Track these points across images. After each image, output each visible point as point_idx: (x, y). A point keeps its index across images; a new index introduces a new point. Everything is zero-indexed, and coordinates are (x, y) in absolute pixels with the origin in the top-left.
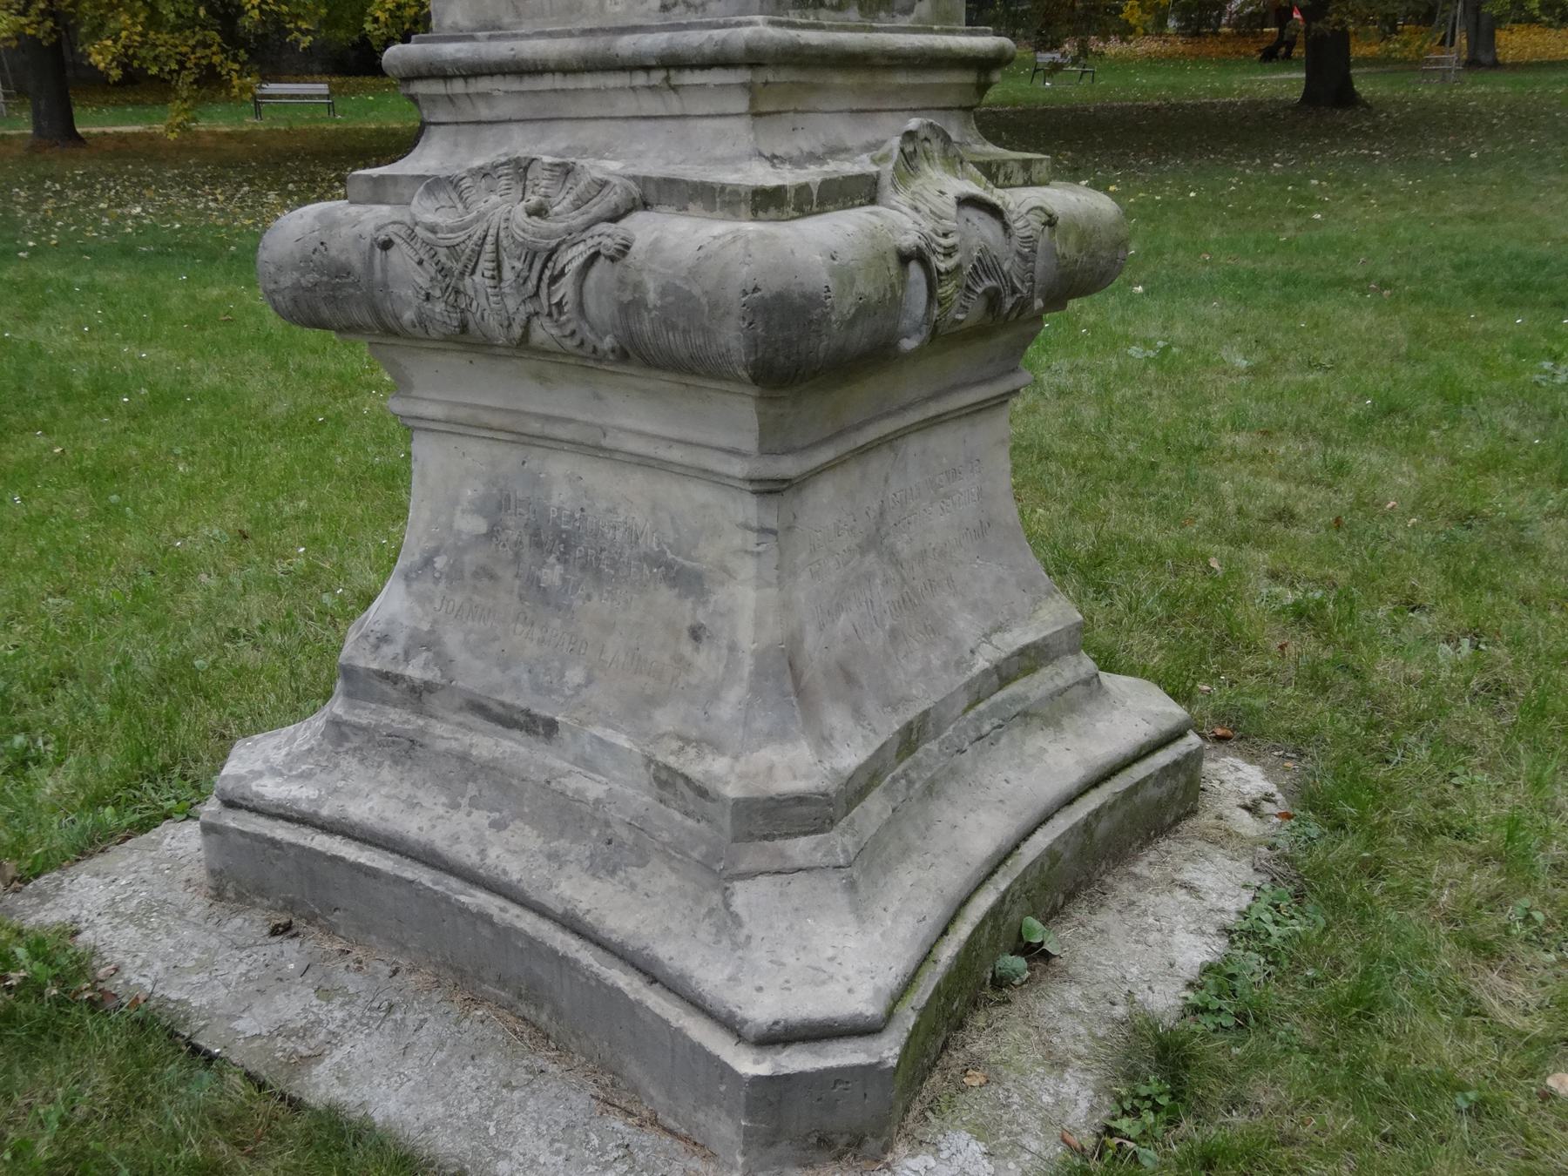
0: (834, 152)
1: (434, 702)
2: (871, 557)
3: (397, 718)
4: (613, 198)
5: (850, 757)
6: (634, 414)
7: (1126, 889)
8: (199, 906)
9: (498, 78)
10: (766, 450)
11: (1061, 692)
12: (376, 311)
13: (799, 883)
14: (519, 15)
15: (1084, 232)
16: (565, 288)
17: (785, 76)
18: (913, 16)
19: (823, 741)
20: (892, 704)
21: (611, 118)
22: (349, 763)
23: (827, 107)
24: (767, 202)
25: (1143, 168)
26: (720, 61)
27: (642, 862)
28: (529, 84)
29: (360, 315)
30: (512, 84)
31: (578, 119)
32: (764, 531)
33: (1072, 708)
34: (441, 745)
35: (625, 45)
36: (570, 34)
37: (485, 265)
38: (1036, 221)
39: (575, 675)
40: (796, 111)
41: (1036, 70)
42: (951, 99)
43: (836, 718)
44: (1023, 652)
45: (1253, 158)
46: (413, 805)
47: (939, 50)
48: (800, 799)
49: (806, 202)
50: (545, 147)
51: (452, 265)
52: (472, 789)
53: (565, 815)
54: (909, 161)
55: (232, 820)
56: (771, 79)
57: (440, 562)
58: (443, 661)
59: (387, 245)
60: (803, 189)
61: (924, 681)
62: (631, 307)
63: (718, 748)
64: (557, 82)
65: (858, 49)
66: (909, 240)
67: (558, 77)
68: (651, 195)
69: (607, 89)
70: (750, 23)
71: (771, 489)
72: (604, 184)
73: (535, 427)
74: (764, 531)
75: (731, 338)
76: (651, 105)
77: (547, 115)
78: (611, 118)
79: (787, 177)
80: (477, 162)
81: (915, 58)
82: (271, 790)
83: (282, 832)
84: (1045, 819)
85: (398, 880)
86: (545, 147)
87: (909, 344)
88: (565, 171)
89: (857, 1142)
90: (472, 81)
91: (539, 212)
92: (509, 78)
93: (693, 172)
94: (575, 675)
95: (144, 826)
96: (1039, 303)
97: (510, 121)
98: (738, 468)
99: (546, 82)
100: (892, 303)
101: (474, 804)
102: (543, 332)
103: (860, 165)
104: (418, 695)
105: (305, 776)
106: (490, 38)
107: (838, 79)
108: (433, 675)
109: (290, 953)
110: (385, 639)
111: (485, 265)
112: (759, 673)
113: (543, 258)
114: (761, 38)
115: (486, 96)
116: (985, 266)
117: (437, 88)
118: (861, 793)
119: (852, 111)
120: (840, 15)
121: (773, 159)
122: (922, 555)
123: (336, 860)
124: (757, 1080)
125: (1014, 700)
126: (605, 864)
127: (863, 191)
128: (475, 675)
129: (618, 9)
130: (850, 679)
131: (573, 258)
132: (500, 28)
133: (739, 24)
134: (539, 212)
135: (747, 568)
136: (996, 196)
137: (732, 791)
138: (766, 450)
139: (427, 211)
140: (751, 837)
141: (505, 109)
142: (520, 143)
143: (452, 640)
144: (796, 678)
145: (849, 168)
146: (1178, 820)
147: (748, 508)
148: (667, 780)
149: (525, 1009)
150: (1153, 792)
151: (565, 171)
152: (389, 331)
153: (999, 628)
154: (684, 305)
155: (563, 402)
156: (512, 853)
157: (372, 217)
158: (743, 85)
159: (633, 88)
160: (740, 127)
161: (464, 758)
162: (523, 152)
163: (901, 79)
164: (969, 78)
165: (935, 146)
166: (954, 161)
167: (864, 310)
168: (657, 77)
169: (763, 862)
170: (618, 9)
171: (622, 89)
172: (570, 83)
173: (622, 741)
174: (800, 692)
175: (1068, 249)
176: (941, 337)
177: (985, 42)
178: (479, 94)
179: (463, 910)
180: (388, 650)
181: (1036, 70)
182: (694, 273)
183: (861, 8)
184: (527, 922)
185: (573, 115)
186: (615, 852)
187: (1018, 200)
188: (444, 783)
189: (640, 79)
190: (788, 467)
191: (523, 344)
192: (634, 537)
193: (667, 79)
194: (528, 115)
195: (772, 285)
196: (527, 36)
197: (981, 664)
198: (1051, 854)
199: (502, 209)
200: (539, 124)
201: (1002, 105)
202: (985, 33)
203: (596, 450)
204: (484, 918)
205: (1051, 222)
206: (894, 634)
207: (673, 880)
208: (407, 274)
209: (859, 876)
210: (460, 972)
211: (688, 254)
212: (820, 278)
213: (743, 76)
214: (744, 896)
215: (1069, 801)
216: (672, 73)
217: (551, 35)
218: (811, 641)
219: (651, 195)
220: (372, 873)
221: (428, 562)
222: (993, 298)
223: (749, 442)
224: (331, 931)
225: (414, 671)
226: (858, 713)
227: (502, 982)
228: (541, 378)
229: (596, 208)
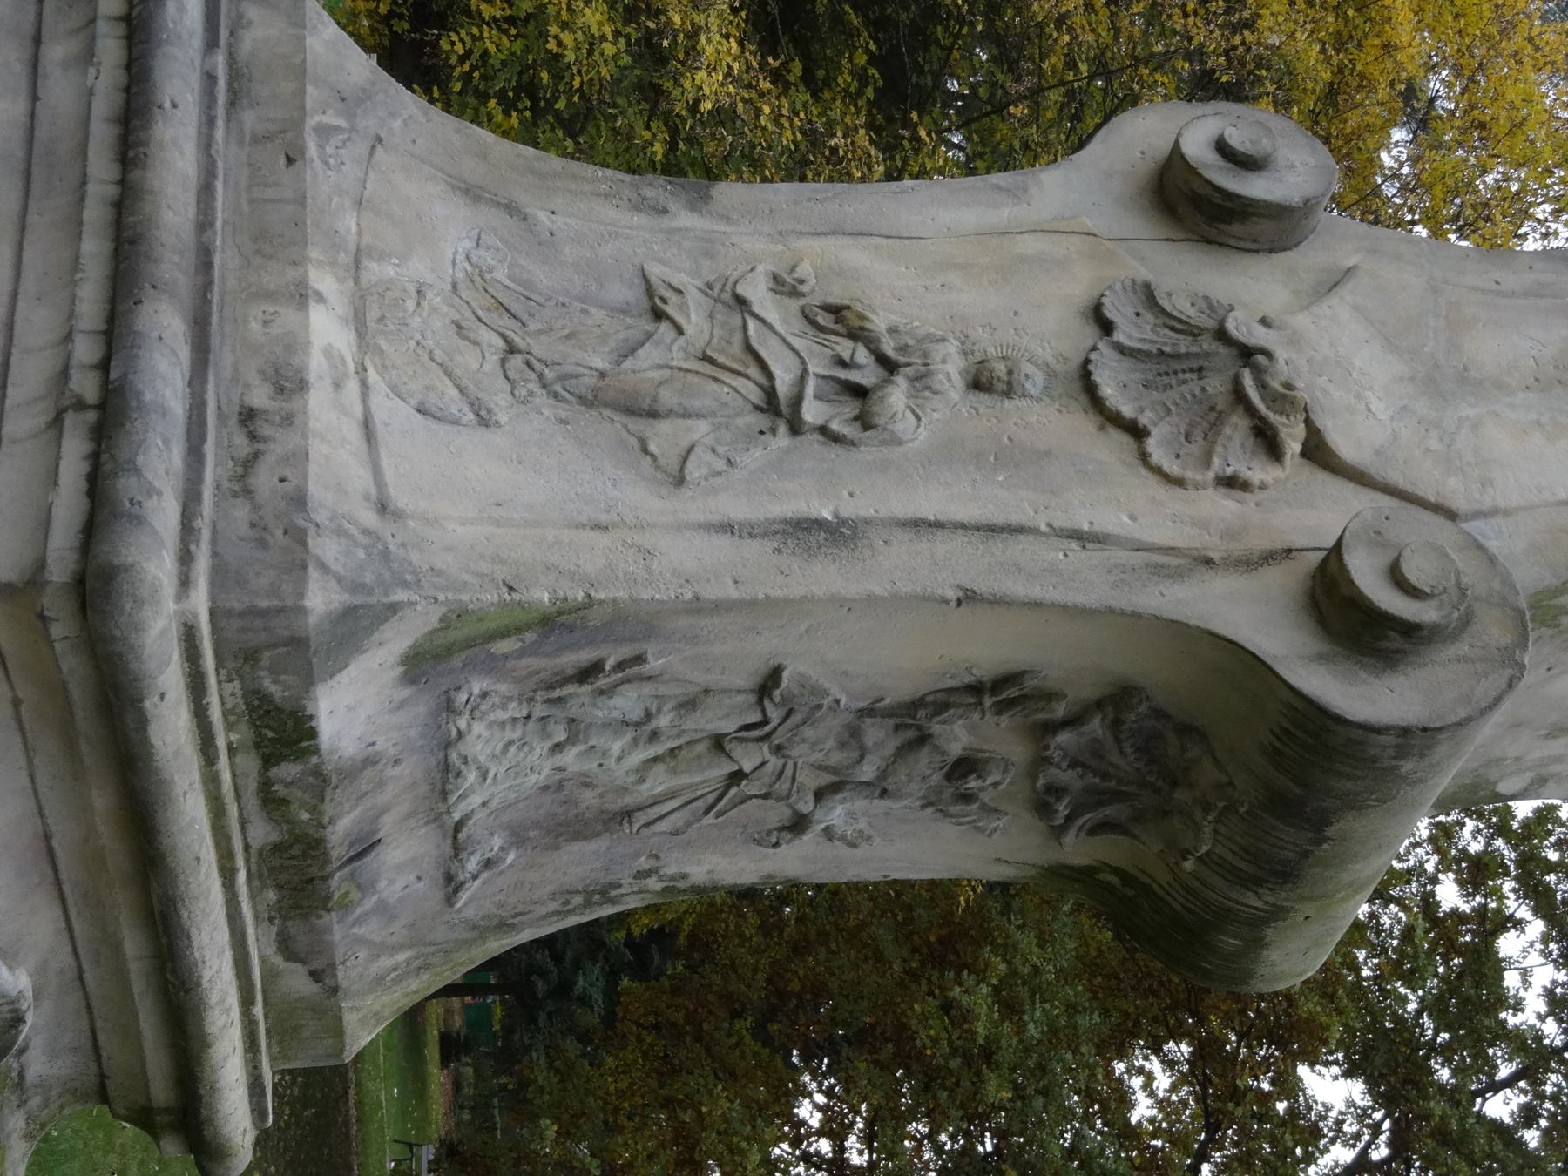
9: (121, 77)
14: (255, 140)
18: (278, 961)
21: (14, 295)
23: (43, 781)
26: (103, 508)
28: (102, 134)
30: (104, 104)
31: (23, 229)
35: (164, 324)
36: (204, 223)
40: (16, 703)
41: (410, 1145)
47: (201, 1025)
56: (57, 630)
65: (166, 842)
67: (112, 191)
69: (74, 283)
70: (185, 583)
77: (35, 169)
78: (14, 295)
81: (174, 971)
90: (121, 29)
92: (120, 98)
97: (35, 98)
99: (101, 169)
106: (210, 78)
107: (102, 799)
114: (139, 603)
115: (88, 56)
119: (47, 837)
120: (252, 802)
129: (255, 326)
132: (232, 103)
133: (185, 558)
141: (60, 91)
158: (41, 565)
159: (68, 338)
163: (134, 944)
164: (161, 1092)
168: (86, 385)
170: (255, 326)
171: (71, 315)
172: (95, 213)
177: (236, 1118)
178: (92, 40)
181: (410, 1145)
183: (277, 848)
185: (32, 218)
189: (86, 350)
193: (80, 405)
194: (42, 133)
196: (206, 144)
200: (20, 153)
201: (359, 1104)
202: (258, 1112)
216: (92, 416)
217: (206, 190)
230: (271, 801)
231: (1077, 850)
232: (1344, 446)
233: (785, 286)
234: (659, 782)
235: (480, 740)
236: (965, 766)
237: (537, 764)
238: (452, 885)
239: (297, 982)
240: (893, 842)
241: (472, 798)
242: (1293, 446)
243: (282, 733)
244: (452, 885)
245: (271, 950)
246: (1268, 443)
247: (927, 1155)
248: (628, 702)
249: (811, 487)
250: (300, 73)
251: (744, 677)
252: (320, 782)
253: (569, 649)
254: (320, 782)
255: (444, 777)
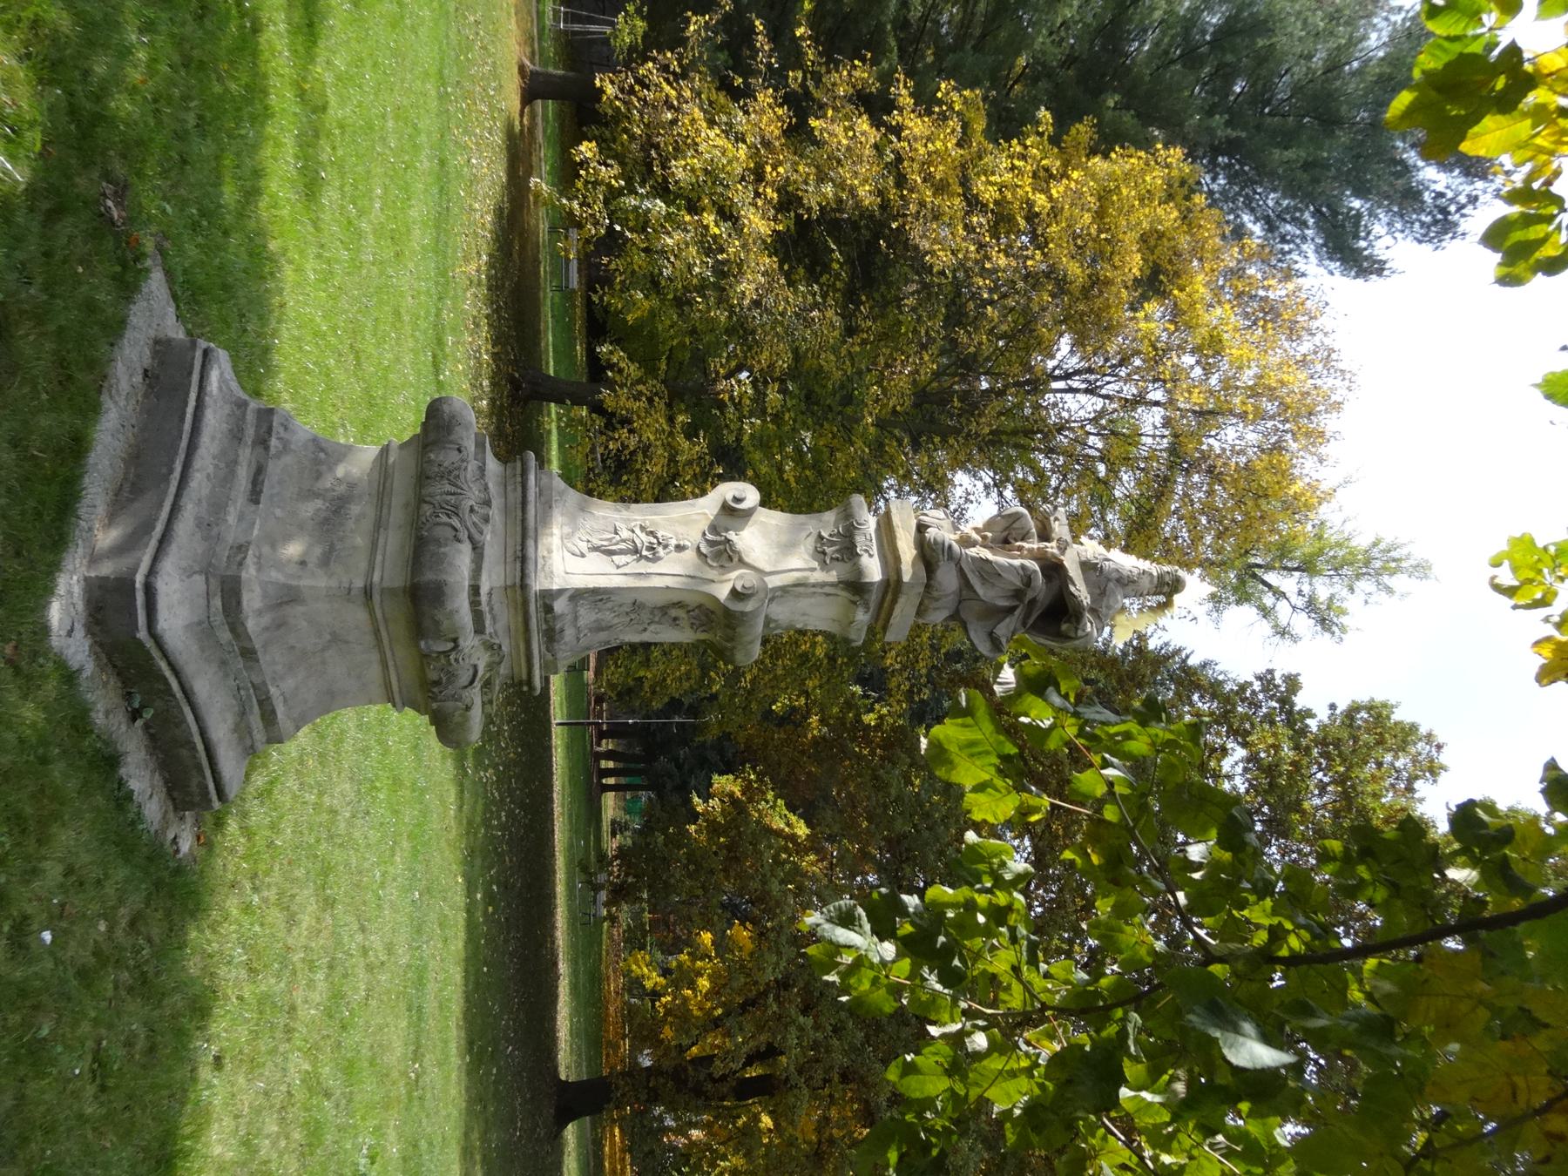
0: (494, 618)
1: (260, 450)
2: (328, 637)
3: (250, 432)
4: (476, 536)
5: (252, 625)
6: (394, 541)
7: (152, 766)
8: (152, 333)
10: (383, 591)
11: (250, 733)
12: (434, 443)
13: (203, 602)
15: (463, 725)
16: (444, 519)
17: (519, 599)
19: (260, 613)
20: (265, 646)
22: (227, 409)
24: (475, 590)
25: (506, 941)
27: (205, 539)
28: (519, 506)
29: (432, 436)
30: (519, 500)
32: (350, 590)
33: (241, 739)
34: (240, 452)
37: (453, 489)
38: (468, 701)
39: (278, 512)
42: (516, 670)
43: (266, 619)
44: (274, 712)
45: (515, 1032)
46: (213, 438)
48: (239, 603)
49: (475, 603)
50: (495, 513)
51: (451, 475)
52: (222, 465)
53: (218, 507)
54: (490, 647)
55: (199, 354)
57: (322, 455)
58: (278, 455)
59: (459, 450)
60: (479, 603)
61: (272, 660)
62: (438, 543)
63: (259, 570)
64: (519, 518)
66: (461, 642)
68: (477, 549)
71: (368, 592)
72: (481, 533)
73: (386, 501)
74: (350, 590)
75: (429, 576)
76: (510, 552)
79: (484, 598)
80: (490, 485)
82: (214, 376)
83: (195, 377)
84: (197, 718)
85: (181, 432)
86: (495, 513)
87: (422, 644)
88: (486, 520)
89: (98, 622)
91: (472, 510)
93: (486, 565)
94: (278, 512)
95: (175, 297)
96: (435, 706)
98: (376, 578)
99: (519, 513)
100: (438, 635)
101: (216, 466)
102: (427, 509)
103: (489, 629)
104: (262, 442)
105: (220, 389)
107: (520, 619)
108: (273, 450)
109: (138, 379)
110: (286, 429)
111: (453, 489)
112: (290, 587)
113: (455, 511)
116: (452, 676)
117: (519, 471)
118: (233, 630)
121: (490, 594)
122: (324, 663)
123: (186, 404)
124: (133, 582)
125: (251, 707)
126: (199, 523)
127: (479, 629)
128: (274, 469)
130: (279, 626)
131: (455, 522)
134: (472, 510)
135: (333, 583)
136: (478, 684)
137: (244, 575)
138: (383, 591)
139: (472, 466)
140: (223, 582)
141: (511, 496)
142: (497, 502)
143: (288, 459)
144: (287, 603)
145: (488, 623)
146: (173, 800)
147: (359, 583)
148: (241, 548)
149: (127, 487)
150: (194, 782)
151: (486, 520)
152: (425, 446)
153: (285, 701)
154: (440, 560)
155: (397, 514)
156: (199, 483)
157: (470, 445)
160: (501, 583)
161: (236, 462)
162: (494, 503)
165: (497, 659)
166: (490, 667)
167: (437, 623)
169: (212, 588)
173: (256, 532)
174: (281, 604)
175: (457, 719)
176: (425, 657)
179: (173, 462)
180: (281, 430)
182: (451, 564)
184: (173, 489)
186: (208, 527)
187: (475, 695)
188: (223, 452)
190: (376, 598)
191: (421, 500)
192: (341, 539)
195: (447, 590)
197: (273, 690)
198: (184, 721)
199: (472, 496)
203: (379, 525)
204: (171, 471)
205: (468, 708)
206: (293, 647)
207: (199, 552)
208: (449, 458)
209: (203, 630)
210: (137, 457)
211: (458, 562)
212: (449, 606)
213: (518, 580)
214: (199, 580)
215: (203, 733)
218: (300, 609)
219: (477, 549)
220: (182, 419)
221: (322, 450)
222: (437, 683)
223: (386, 584)
224: (146, 396)
225: (274, 442)
226: (266, 629)
227: (138, 476)
228: (407, 505)
229: (473, 530)
230: (546, 621)
231: (703, 636)
232: (746, 559)
233: (642, 528)
234: (616, 621)
235: (582, 611)
236: (675, 619)
237: (593, 617)
238: (578, 639)
239: (549, 656)
240: (667, 635)
241: (581, 623)
242: (736, 559)
243: (549, 609)
244: (578, 639)
245: (543, 648)
246: (731, 559)
247: (1420, 1138)
248: (609, 605)
249: (644, 567)
250: (551, 489)
251: (630, 601)
252: (555, 618)
253: (597, 596)
254: (555, 618)
255: (576, 618)
